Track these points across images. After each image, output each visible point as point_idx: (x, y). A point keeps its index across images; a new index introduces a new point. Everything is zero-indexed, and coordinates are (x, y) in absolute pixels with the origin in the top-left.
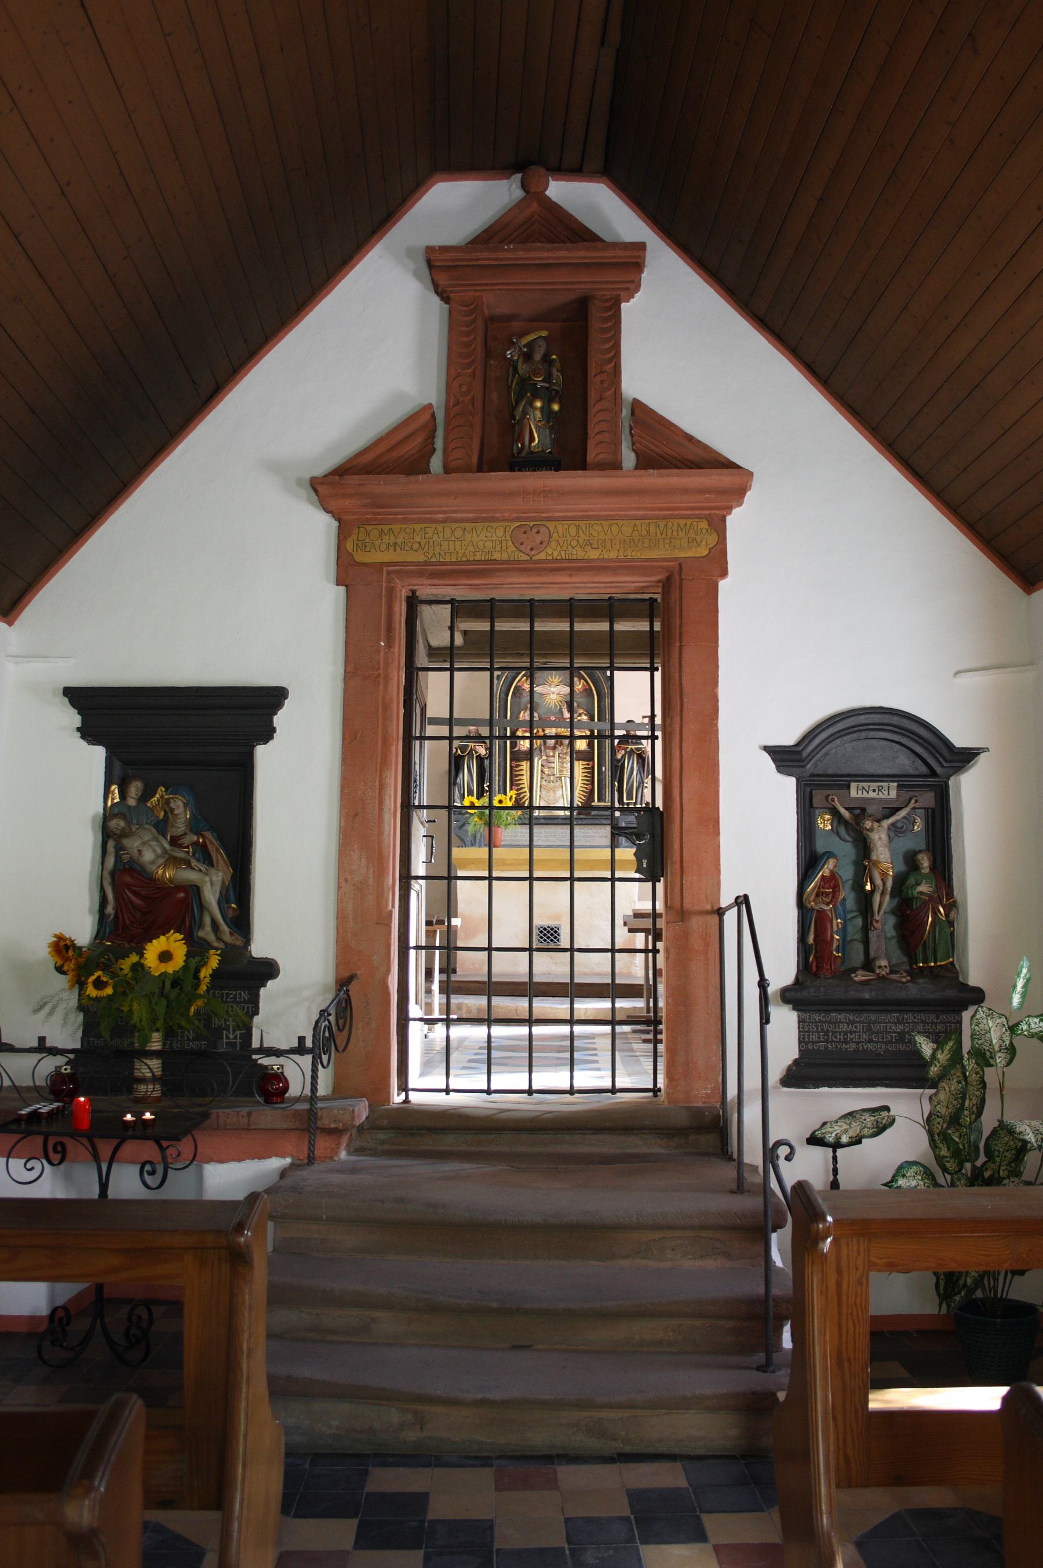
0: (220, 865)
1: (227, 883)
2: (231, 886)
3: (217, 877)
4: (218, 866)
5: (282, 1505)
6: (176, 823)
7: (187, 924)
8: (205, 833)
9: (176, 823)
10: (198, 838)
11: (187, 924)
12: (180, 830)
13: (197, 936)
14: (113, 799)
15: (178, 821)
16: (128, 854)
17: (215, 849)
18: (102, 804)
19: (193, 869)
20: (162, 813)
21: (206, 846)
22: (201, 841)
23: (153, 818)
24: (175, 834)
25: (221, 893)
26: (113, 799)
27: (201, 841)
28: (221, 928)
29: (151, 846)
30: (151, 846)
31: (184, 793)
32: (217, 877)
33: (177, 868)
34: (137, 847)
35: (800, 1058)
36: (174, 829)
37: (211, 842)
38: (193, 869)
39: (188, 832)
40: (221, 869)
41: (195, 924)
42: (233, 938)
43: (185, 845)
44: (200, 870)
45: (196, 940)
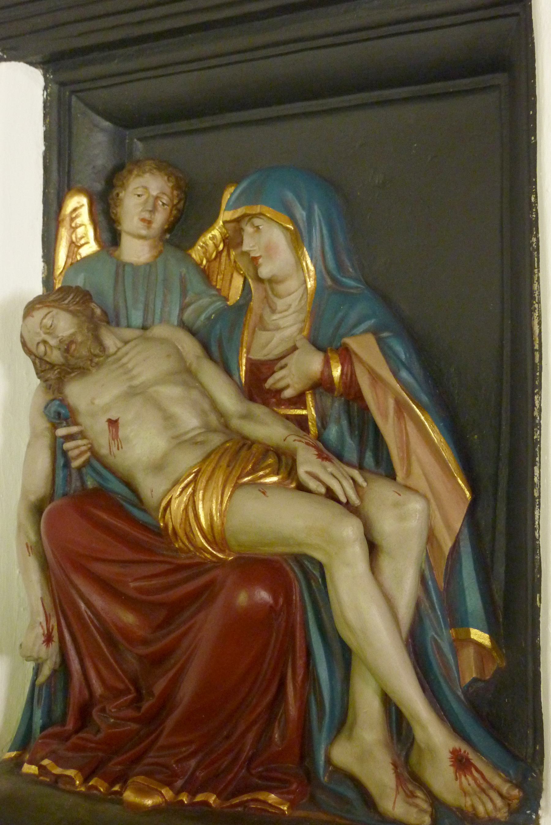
0: (416, 470)
1: (447, 544)
2: (466, 531)
3: (402, 518)
4: (408, 473)
5: (536, 161)
6: (273, 311)
7: (293, 710)
8: (352, 343)
9: (273, 311)
10: (327, 364)
11: (293, 710)
12: (278, 336)
13: (328, 761)
14: (74, 246)
15: (280, 304)
16: (82, 435)
17: (391, 403)
18: (39, 265)
19: (302, 488)
20: (238, 282)
21: (359, 396)
22: (337, 372)
23: (205, 301)
24: (258, 355)
25: (423, 580)
26: (74, 246)
27: (337, 372)
28: (419, 734)
29: (158, 406)
30: (158, 406)
31: (290, 196)
32: (402, 518)
33: (237, 486)
34: (106, 408)
35: (46, 149)
36: (262, 336)
37: (375, 378)
38: (302, 488)
39: (302, 343)
40: (422, 485)
41: (321, 718)
42: (467, 781)
43: (288, 393)
44: (330, 495)
45: (325, 779)
